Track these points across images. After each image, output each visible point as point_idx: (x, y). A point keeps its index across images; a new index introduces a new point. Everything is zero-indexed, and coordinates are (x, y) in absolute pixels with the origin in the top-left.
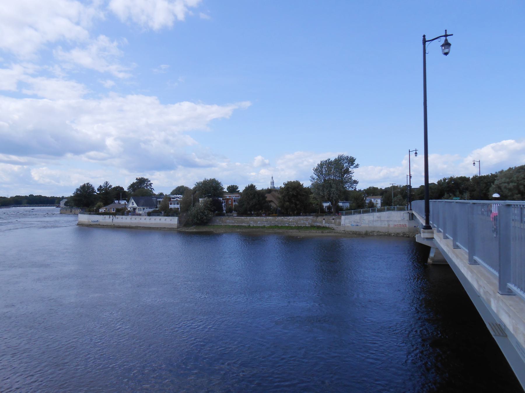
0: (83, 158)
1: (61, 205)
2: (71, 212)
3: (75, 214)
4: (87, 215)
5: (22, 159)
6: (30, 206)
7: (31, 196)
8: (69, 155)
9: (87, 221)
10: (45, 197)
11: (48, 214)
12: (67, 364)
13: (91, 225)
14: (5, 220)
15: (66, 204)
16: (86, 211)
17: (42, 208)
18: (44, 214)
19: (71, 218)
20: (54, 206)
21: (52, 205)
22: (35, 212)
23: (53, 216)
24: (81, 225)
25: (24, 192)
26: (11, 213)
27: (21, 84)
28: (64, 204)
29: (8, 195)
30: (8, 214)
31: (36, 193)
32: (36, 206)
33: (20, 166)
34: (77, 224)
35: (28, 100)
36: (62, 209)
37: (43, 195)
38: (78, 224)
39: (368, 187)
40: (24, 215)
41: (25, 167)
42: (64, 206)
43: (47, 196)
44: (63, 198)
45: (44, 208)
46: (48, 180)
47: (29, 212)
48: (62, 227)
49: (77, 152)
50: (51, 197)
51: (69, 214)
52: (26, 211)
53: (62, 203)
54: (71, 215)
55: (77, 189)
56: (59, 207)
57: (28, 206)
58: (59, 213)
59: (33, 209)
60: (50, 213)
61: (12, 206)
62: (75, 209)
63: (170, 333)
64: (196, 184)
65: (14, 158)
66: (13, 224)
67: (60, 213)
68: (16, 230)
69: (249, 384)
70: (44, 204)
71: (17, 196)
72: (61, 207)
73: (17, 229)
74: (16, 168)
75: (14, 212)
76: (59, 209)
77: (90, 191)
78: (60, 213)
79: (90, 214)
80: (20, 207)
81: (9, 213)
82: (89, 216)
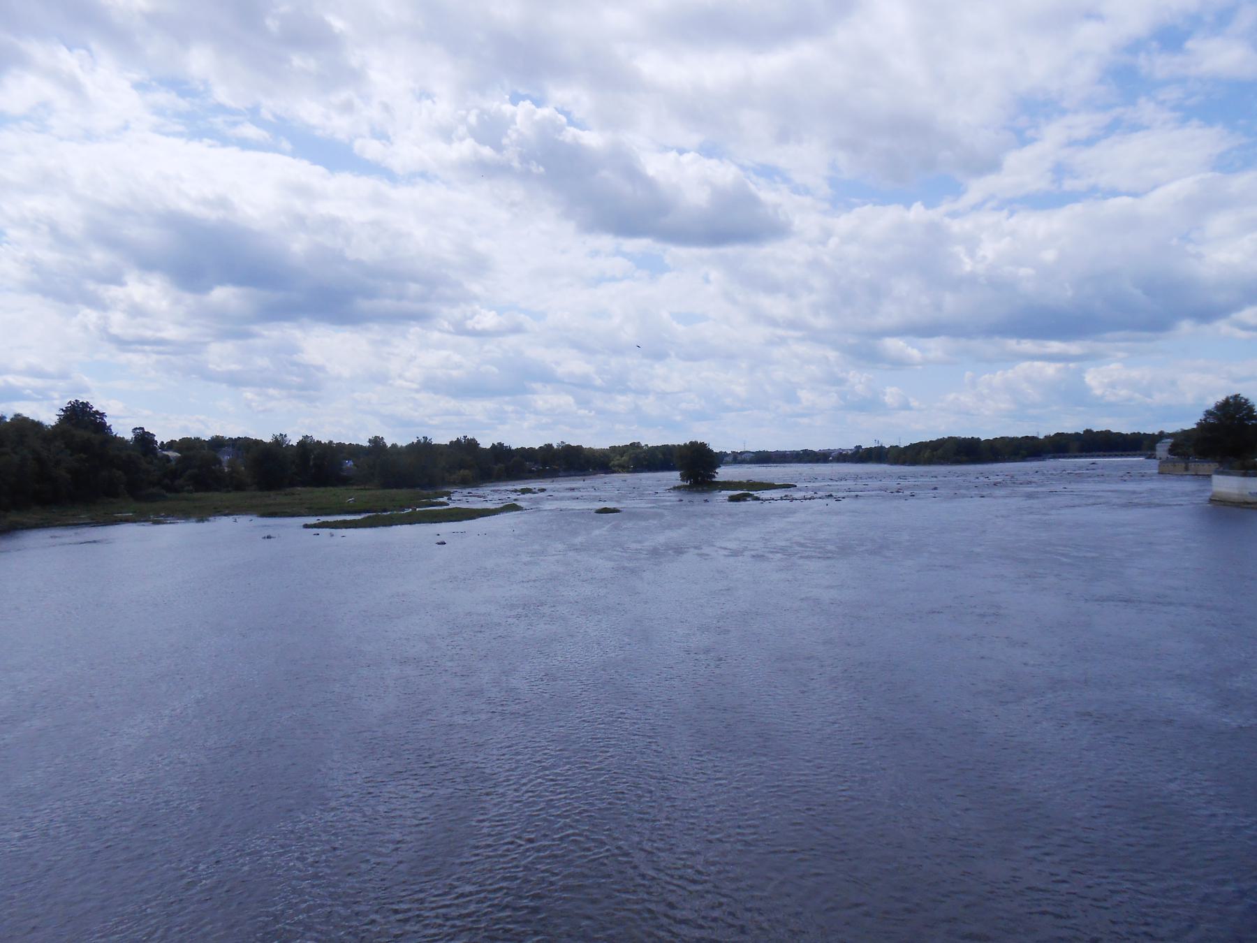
0: (1222, 327)
1: (1157, 453)
2: (1187, 469)
3: (1196, 475)
4: (1235, 478)
5: (1074, 348)
6: (1086, 457)
7: (1088, 432)
8: (1186, 326)
9: (1236, 492)
10: (1119, 434)
11: (1128, 476)
12: (731, 817)
13: (1248, 503)
14: (1041, 486)
15: (1173, 450)
16: (1232, 468)
17: (1114, 461)
18: (1121, 473)
19: (1188, 485)
20: (1140, 455)
21: (1061, 454)
22: (1099, 468)
23: (1143, 478)
24: (1220, 504)
25: (1072, 425)
26: (1050, 472)
27: (1060, 171)
28: (1169, 450)
29: (1038, 433)
30: (1043, 474)
31: (1100, 424)
32: (1098, 456)
33: (1060, 365)
34: (1208, 498)
35: (1078, 208)
36: (1163, 462)
37: (1114, 431)
38: (1211, 501)
39: (942, 437)
40: (1078, 477)
41: (1072, 365)
42: (1169, 456)
43: (1124, 432)
44: (1162, 435)
45: (1117, 461)
46: (1123, 393)
47: (1087, 469)
48: (1170, 505)
49: (1206, 314)
50: (1131, 434)
51: (1182, 475)
52: (1080, 468)
53: (1162, 450)
54: (1188, 477)
55: (1207, 411)
56: (1153, 456)
57: (1081, 457)
58: (1157, 471)
59: (1093, 464)
60: (1133, 473)
61: (1050, 455)
62: (1198, 462)
63: (501, 791)
64: (1245, 405)
65: (1055, 346)
66: (1059, 495)
67: (1159, 473)
68: (94, 545)
69: (345, 938)
70: (1117, 450)
71: (1058, 434)
72: (1158, 457)
73: (95, 542)
74: (1051, 369)
75: (1055, 470)
76: (1154, 463)
77: (1243, 416)
78: (1159, 473)
79: (1245, 475)
80: (1064, 457)
81: (1045, 472)
82: (1242, 479)
